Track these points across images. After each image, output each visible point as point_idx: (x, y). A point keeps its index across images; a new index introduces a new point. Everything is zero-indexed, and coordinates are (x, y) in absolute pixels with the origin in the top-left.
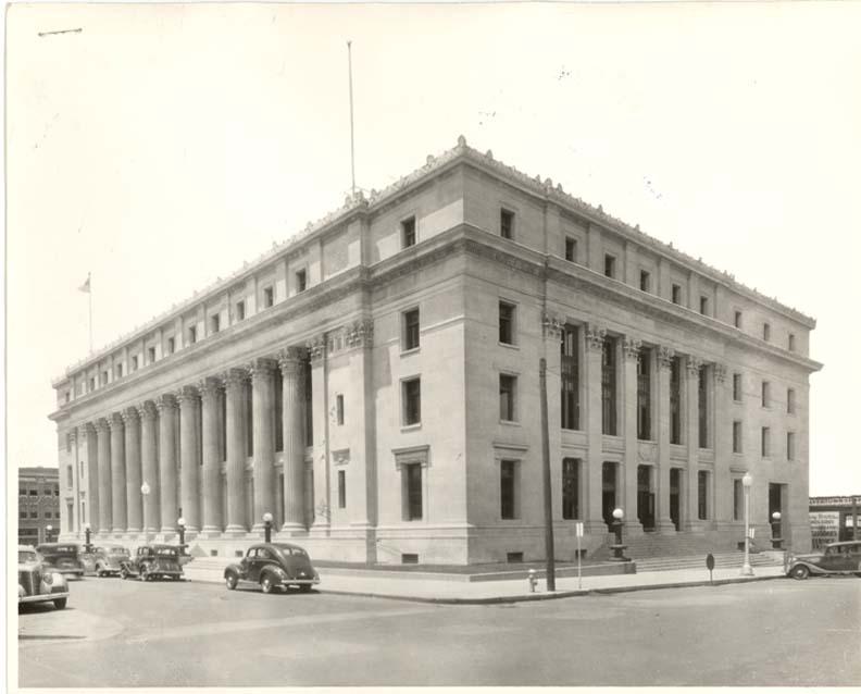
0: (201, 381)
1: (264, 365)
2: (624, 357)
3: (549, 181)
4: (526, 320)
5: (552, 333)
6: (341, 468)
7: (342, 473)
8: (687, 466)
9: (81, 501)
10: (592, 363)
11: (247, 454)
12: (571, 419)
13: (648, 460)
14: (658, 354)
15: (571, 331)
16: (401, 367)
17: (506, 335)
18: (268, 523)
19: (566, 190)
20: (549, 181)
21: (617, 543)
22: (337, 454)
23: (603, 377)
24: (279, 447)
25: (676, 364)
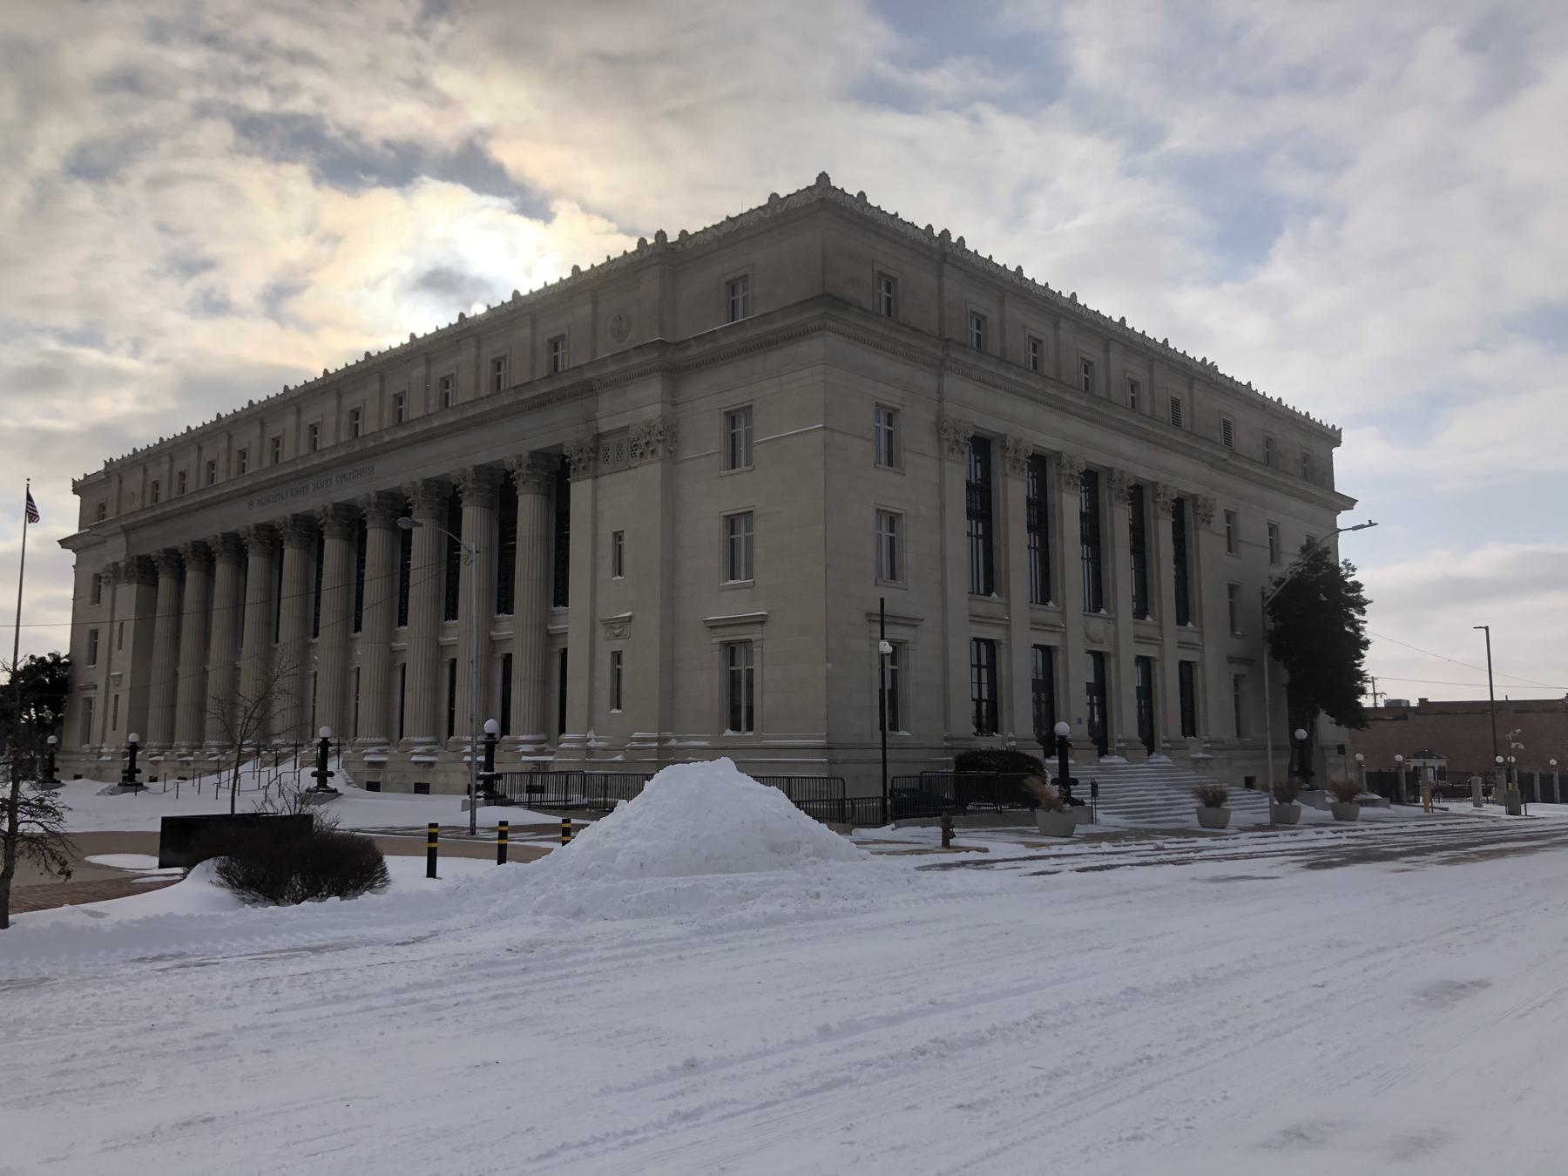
0: (325, 508)
3: (946, 233)
4: (916, 433)
5: (1119, 497)
6: (617, 645)
7: (617, 657)
8: (1009, 638)
10: (1014, 493)
11: (352, 627)
12: (988, 578)
13: (1101, 642)
14: (1157, 495)
15: (981, 446)
16: (732, 493)
17: (891, 457)
19: (872, 200)
20: (946, 233)
22: (609, 624)
23: (1029, 515)
24: (452, 612)
25: (1137, 494)
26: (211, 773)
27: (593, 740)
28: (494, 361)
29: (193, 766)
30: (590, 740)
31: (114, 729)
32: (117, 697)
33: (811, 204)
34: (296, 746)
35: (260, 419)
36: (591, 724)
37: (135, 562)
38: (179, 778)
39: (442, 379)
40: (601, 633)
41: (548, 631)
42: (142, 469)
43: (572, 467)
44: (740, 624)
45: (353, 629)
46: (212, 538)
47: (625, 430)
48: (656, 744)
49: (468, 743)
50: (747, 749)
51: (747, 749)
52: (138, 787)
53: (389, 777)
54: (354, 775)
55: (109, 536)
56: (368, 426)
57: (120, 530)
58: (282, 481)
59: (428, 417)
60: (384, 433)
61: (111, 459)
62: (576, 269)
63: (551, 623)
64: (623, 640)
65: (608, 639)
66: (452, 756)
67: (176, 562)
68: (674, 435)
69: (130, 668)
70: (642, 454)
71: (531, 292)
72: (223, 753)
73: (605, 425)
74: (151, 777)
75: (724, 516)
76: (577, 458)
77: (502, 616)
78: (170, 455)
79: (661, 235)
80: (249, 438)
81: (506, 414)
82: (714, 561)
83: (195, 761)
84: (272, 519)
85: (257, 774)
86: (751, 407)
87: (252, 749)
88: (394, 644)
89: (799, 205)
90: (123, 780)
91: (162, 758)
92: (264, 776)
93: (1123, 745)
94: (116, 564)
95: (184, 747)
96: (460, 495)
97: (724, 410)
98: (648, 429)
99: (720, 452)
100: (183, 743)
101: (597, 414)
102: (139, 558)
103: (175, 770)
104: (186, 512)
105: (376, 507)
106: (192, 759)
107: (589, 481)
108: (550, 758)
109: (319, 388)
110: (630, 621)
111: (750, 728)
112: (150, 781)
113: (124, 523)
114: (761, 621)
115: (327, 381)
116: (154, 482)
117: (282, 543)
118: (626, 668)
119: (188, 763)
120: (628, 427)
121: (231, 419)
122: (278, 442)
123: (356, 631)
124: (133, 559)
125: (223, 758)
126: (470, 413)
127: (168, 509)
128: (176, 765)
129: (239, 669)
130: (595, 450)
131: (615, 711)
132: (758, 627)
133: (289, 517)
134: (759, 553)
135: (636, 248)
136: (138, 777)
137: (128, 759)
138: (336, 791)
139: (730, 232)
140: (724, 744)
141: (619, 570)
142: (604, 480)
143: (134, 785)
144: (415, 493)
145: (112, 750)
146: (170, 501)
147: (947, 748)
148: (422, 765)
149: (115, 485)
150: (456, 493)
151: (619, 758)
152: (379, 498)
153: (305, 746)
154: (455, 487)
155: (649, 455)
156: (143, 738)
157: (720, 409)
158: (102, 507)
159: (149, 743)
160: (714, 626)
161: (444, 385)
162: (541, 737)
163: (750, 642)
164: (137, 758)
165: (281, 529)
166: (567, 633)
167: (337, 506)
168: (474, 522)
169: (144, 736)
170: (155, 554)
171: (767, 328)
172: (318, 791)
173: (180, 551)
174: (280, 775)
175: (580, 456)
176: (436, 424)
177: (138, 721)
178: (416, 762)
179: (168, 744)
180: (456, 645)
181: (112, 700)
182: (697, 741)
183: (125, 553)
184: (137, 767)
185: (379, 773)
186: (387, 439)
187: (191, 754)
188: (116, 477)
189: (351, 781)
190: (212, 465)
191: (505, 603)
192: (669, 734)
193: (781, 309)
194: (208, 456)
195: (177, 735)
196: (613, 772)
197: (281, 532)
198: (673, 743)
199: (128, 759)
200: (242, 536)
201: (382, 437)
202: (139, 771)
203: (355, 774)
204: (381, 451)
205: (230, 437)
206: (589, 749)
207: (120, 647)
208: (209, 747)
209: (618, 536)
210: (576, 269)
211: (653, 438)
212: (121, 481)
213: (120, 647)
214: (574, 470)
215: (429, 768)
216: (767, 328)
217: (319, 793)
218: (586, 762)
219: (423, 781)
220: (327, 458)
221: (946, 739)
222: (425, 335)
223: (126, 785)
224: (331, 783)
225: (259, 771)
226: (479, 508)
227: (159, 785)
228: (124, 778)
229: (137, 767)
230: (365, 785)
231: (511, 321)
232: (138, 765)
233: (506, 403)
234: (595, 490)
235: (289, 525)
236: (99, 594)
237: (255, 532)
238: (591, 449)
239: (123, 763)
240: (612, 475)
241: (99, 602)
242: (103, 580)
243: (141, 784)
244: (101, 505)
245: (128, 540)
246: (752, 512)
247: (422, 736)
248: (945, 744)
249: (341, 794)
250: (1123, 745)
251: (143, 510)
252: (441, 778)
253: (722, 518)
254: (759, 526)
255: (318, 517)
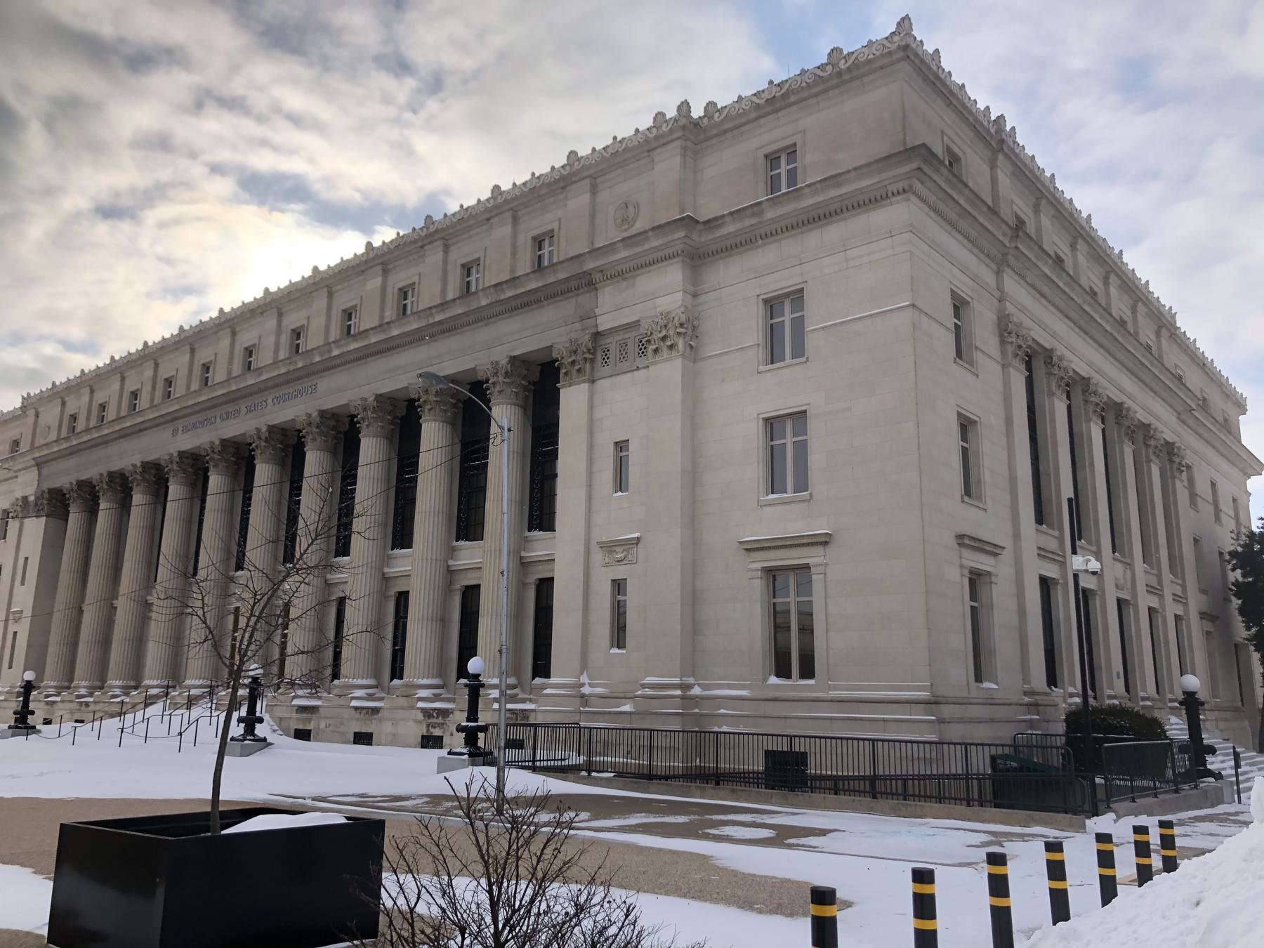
0: (258, 430)
1: (232, 450)
2: (1087, 414)
6: (620, 572)
7: (619, 586)
9: (11, 629)
18: (29, 682)
21: (469, 720)
22: (609, 547)
26: (112, 716)
27: (587, 686)
28: (534, 239)
29: (92, 707)
30: (582, 685)
31: (10, 667)
32: (15, 633)
33: (890, 53)
34: (168, 687)
35: (328, 286)
36: (584, 666)
37: (46, 495)
38: (77, 721)
39: (400, 289)
40: (598, 557)
41: (383, 574)
42: (326, 294)
43: (563, 371)
44: (769, 548)
45: (390, 544)
46: (68, 486)
47: (636, 324)
48: (678, 692)
49: (494, 687)
50: (794, 701)
51: (794, 701)
52: (31, 729)
53: (322, 725)
54: (280, 721)
55: (20, 470)
56: (312, 340)
57: (33, 462)
58: (213, 405)
59: (383, 326)
60: (333, 345)
61: (28, 394)
62: (267, 290)
63: (452, 559)
64: (628, 566)
65: (606, 565)
66: (402, 702)
67: (89, 494)
68: (694, 328)
69: (31, 605)
70: (656, 351)
71: (279, 288)
72: (127, 694)
73: (605, 323)
74: (45, 719)
75: (763, 419)
76: (570, 360)
77: (537, 534)
78: (90, 386)
79: (684, 107)
80: (176, 365)
81: (415, 339)
82: (753, 472)
83: (95, 702)
84: (198, 445)
85: (166, 718)
86: (802, 290)
87: (162, 690)
88: (328, 576)
89: (871, 56)
90: (15, 722)
91: (58, 699)
92: (176, 721)
93: (1149, 703)
94: (25, 498)
95: (84, 687)
96: (358, 425)
97: (762, 297)
98: (495, 371)
99: (758, 345)
100: (84, 683)
101: (596, 310)
102: (50, 491)
103: (72, 713)
104: (105, 442)
105: (266, 440)
106: (92, 699)
107: (584, 387)
108: (532, 707)
109: (236, 317)
110: (637, 544)
111: (808, 671)
112: (44, 724)
113: (37, 455)
114: (823, 542)
115: (182, 337)
116: (72, 416)
117: (167, 480)
118: (632, 600)
119: (87, 704)
120: (639, 321)
121: (65, 386)
122: (208, 368)
123: (237, 570)
124: (43, 492)
125: (127, 700)
126: (438, 318)
127: (86, 438)
128: (74, 706)
129: (116, 608)
130: (592, 351)
131: (615, 651)
132: (819, 550)
133: (217, 442)
134: (816, 460)
135: (490, 196)
136: (31, 720)
137: (21, 699)
138: (265, 740)
139: (774, 97)
140: (770, 695)
141: (621, 483)
142: (603, 384)
143: (25, 728)
144: (365, 410)
145: (6, 690)
146: (87, 430)
147: (1028, 705)
148: (364, 711)
149: (31, 419)
150: (300, 438)
151: (627, 708)
152: (321, 418)
153: (178, 687)
154: (300, 431)
155: (665, 351)
156: (40, 677)
157: (758, 296)
158: (16, 443)
159: (109, 682)
160: (753, 548)
161: (168, 384)
162: (512, 681)
163: (807, 567)
164: (31, 698)
165: (208, 455)
166: (554, 560)
167: (271, 429)
168: (371, 450)
169: (40, 675)
170: (68, 486)
171: (833, 193)
172: (245, 739)
173: (94, 482)
174: (148, 719)
175: (573, 358)
176: (395, 332)
177: (36, 659)
178: (356, 708)
179: (66, 684)
180: (409, 576)
181: (10, 636)
182: (730, 689)
183: (36, 487)
184: (30, 709)
185: (311, 719)
186: (336, 352)
187: (91, 695)
188: (33, 411)
189: (276, 728)
190: (135, 395)
191: (402, 536)
192: (691, 680)
193: (855, 169)
194: (131, 386)
195: (78, 672)
196: (617, 725)
197: (207, 458)
198: (696, 691)
199: (21, 699)
200: (163, 464)
201: (330, 351)
202: (32, 713)
203: (281, 719)
204: (329, 366)
205: (157, 365)
206: (583, 696)
207: (23, 583)
208: (113, 687)
209: (621, 446)
210: (267, 290)
211: (671, 332)
212: (37, 415)
213: (23, 583)
214: (566, 374)
215: (372, 714)
216: (833, 193)
217: (246, 742)
218: (580, 712)
219: (364, 730)
220: (265, 377)
221: (1026, 694)
222: (255, 299)
223: (17, 727)
224: (260, 730)
225: (170, 715)
226: (441, 424)
227: (53, 728)
228: (16, 720)
229: (30, 709)
230: (292, 732)
231: (488, 219)
232: (32, 706)
233: (484, 303)
234: (592, 395)
235: (216, 451)
236: (6, 530)
237: (178, 459)
238: (589, 350)
239: (17, 703)
240: (613, 378)
241: (5, 538)
242: (11, 514)
243: (34, 727)
244: (14, 441)
245: (40, 475)
246: (805, 411)
247: (363, 678)
248: (1027, 699)
249: (271, 744)
250: (1149, 703)
251: (276, 363)
252: (387, 727)
253: (761, 420)
254: (815, 428)
255: (203, 453)
